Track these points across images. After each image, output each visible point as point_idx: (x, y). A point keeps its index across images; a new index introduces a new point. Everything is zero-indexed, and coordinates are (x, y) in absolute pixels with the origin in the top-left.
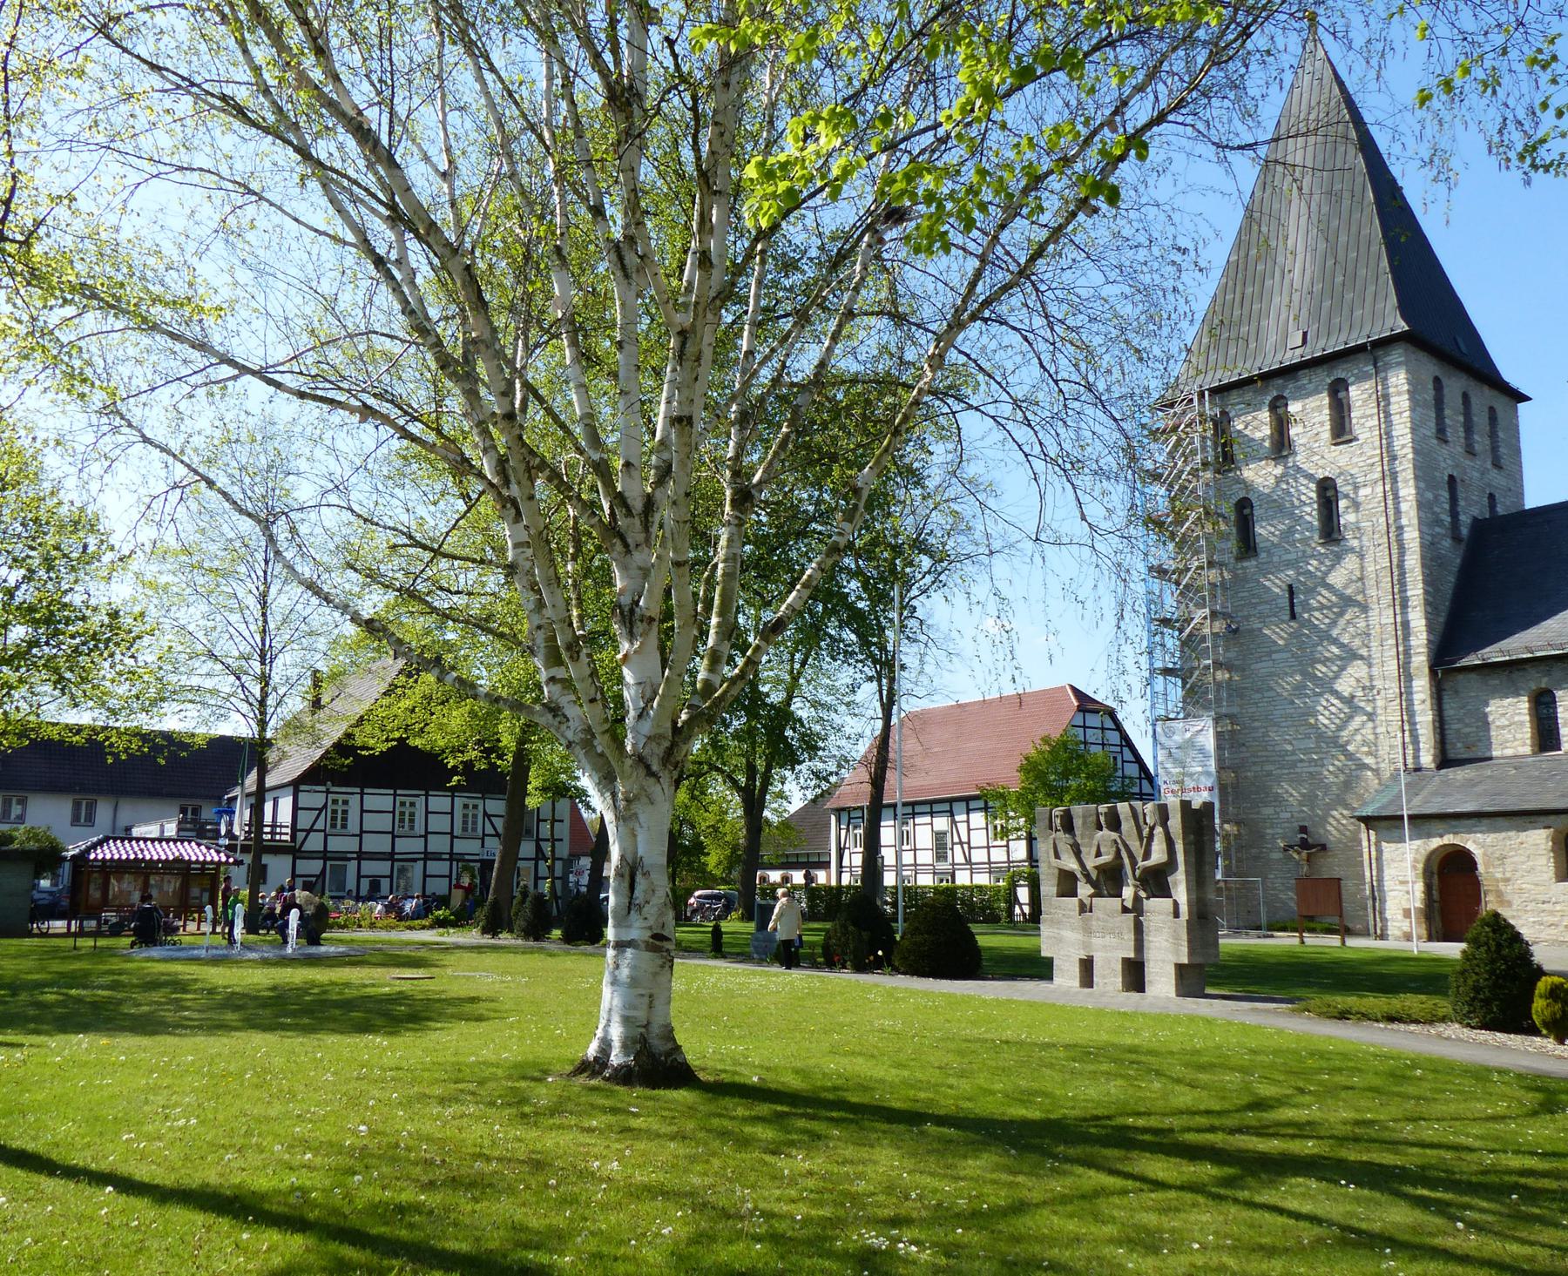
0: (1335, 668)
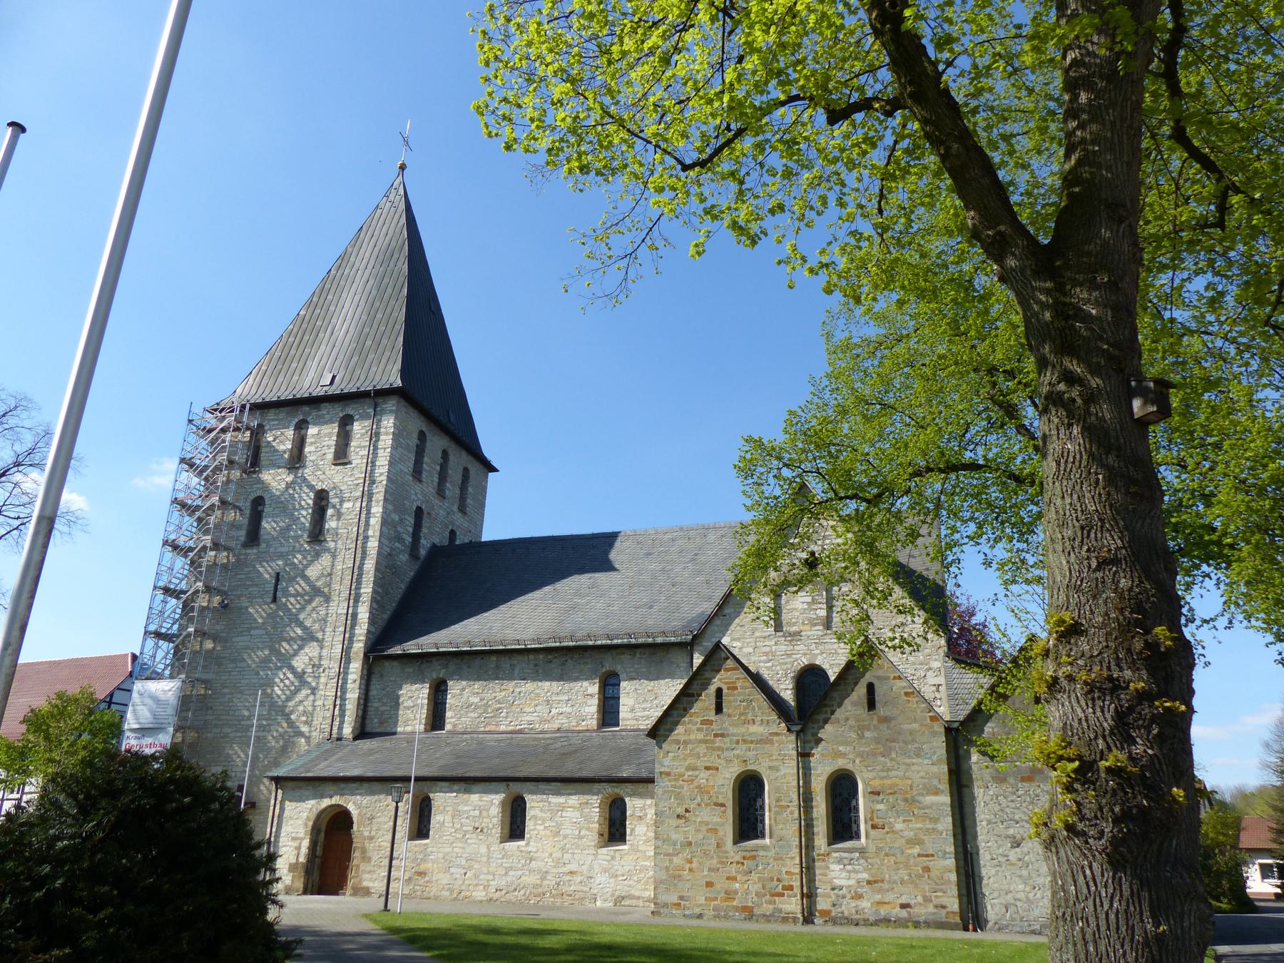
0: (295, 647)
